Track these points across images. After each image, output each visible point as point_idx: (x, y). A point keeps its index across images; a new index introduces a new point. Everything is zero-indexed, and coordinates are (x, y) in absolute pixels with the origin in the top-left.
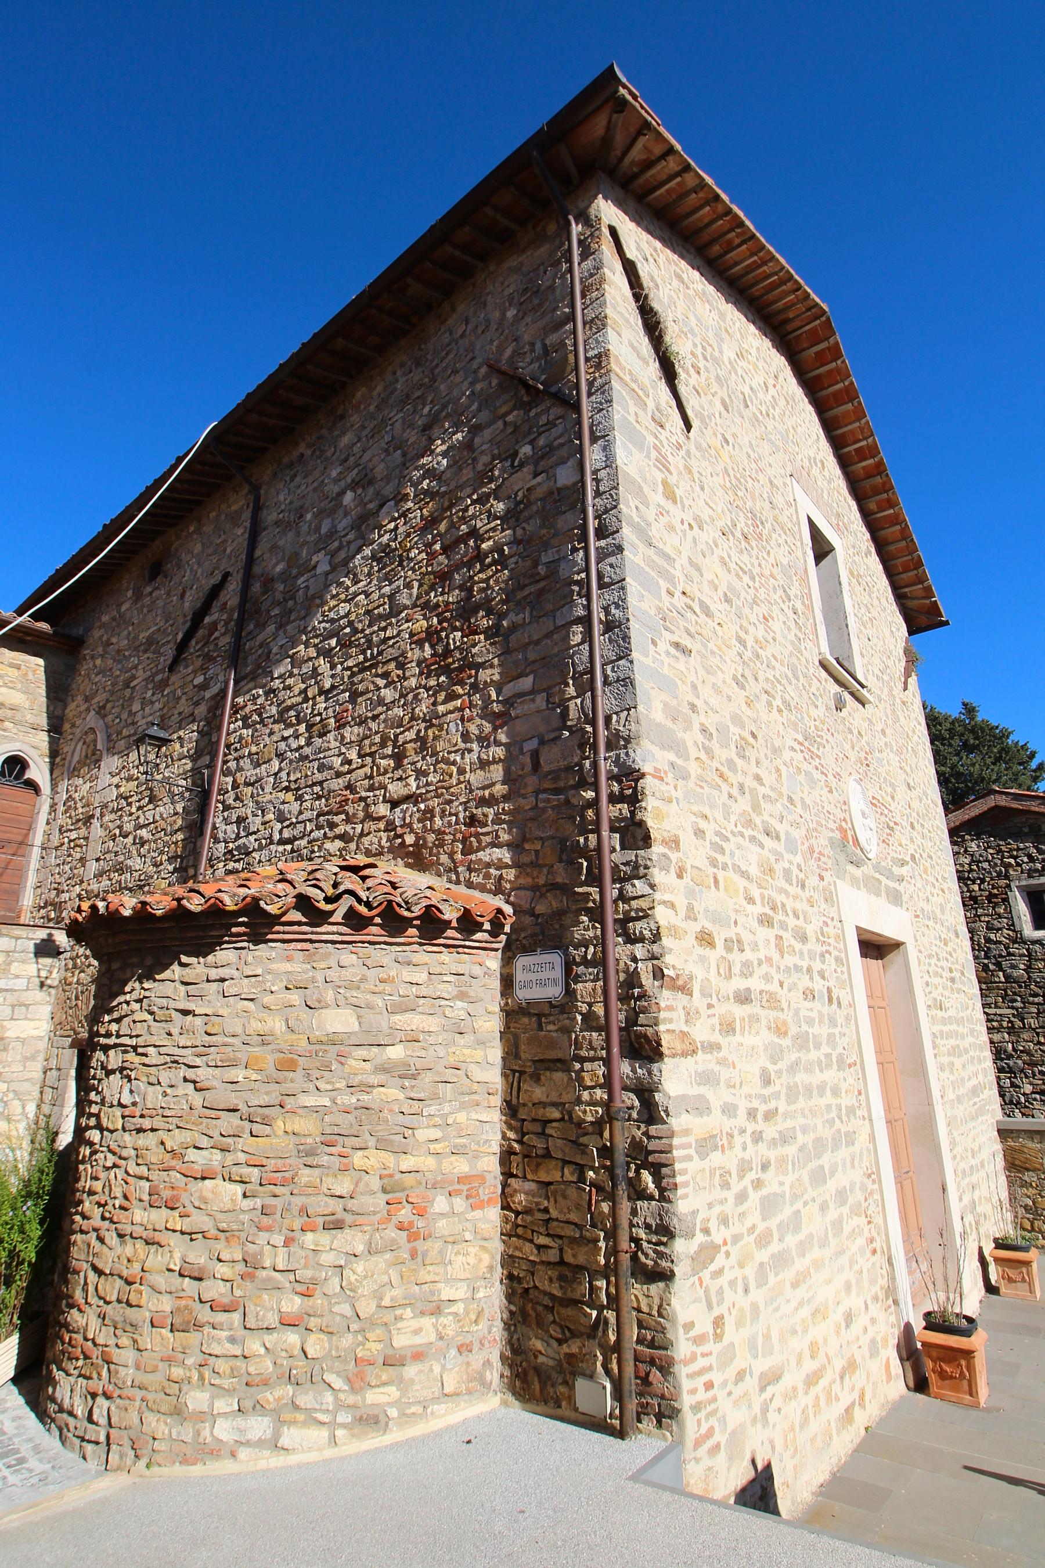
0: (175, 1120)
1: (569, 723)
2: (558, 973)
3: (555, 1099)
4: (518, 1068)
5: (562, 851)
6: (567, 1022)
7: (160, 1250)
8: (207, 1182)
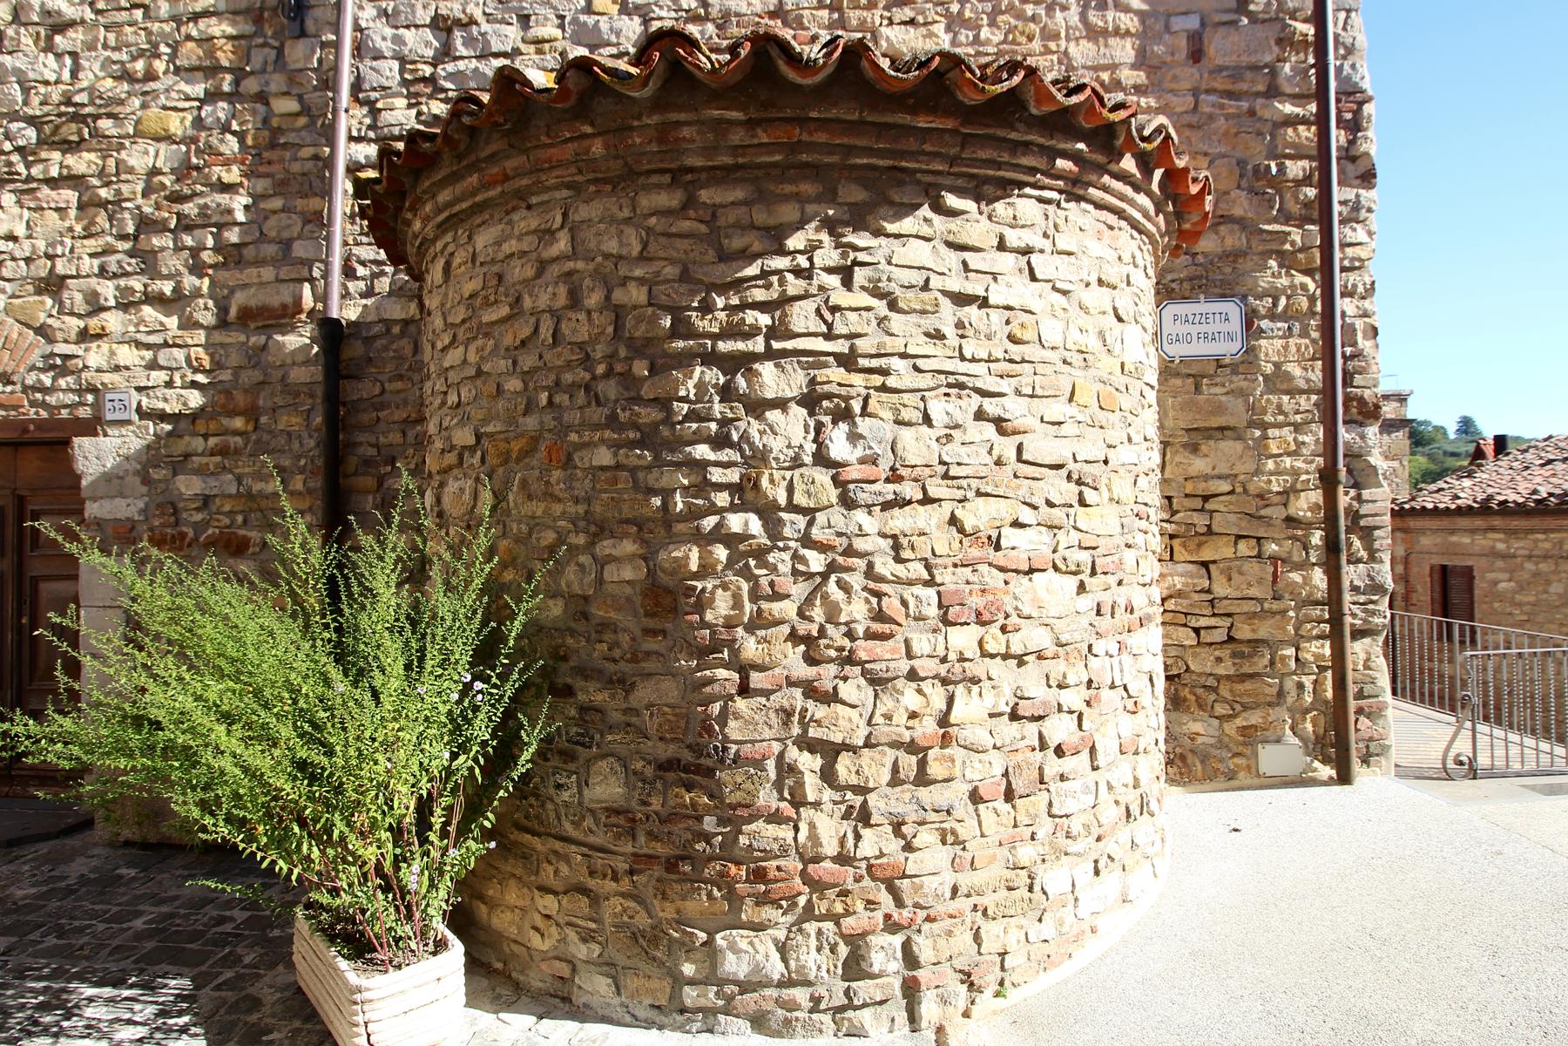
0: (975, 483)
1: (1252, 7)
2: (1235, 325)
3: (1225, 471)
4: (1184, 438)
5: (1241, 176)
6: (1244, 384)
7: (975, 689)
8: (1036, 576)
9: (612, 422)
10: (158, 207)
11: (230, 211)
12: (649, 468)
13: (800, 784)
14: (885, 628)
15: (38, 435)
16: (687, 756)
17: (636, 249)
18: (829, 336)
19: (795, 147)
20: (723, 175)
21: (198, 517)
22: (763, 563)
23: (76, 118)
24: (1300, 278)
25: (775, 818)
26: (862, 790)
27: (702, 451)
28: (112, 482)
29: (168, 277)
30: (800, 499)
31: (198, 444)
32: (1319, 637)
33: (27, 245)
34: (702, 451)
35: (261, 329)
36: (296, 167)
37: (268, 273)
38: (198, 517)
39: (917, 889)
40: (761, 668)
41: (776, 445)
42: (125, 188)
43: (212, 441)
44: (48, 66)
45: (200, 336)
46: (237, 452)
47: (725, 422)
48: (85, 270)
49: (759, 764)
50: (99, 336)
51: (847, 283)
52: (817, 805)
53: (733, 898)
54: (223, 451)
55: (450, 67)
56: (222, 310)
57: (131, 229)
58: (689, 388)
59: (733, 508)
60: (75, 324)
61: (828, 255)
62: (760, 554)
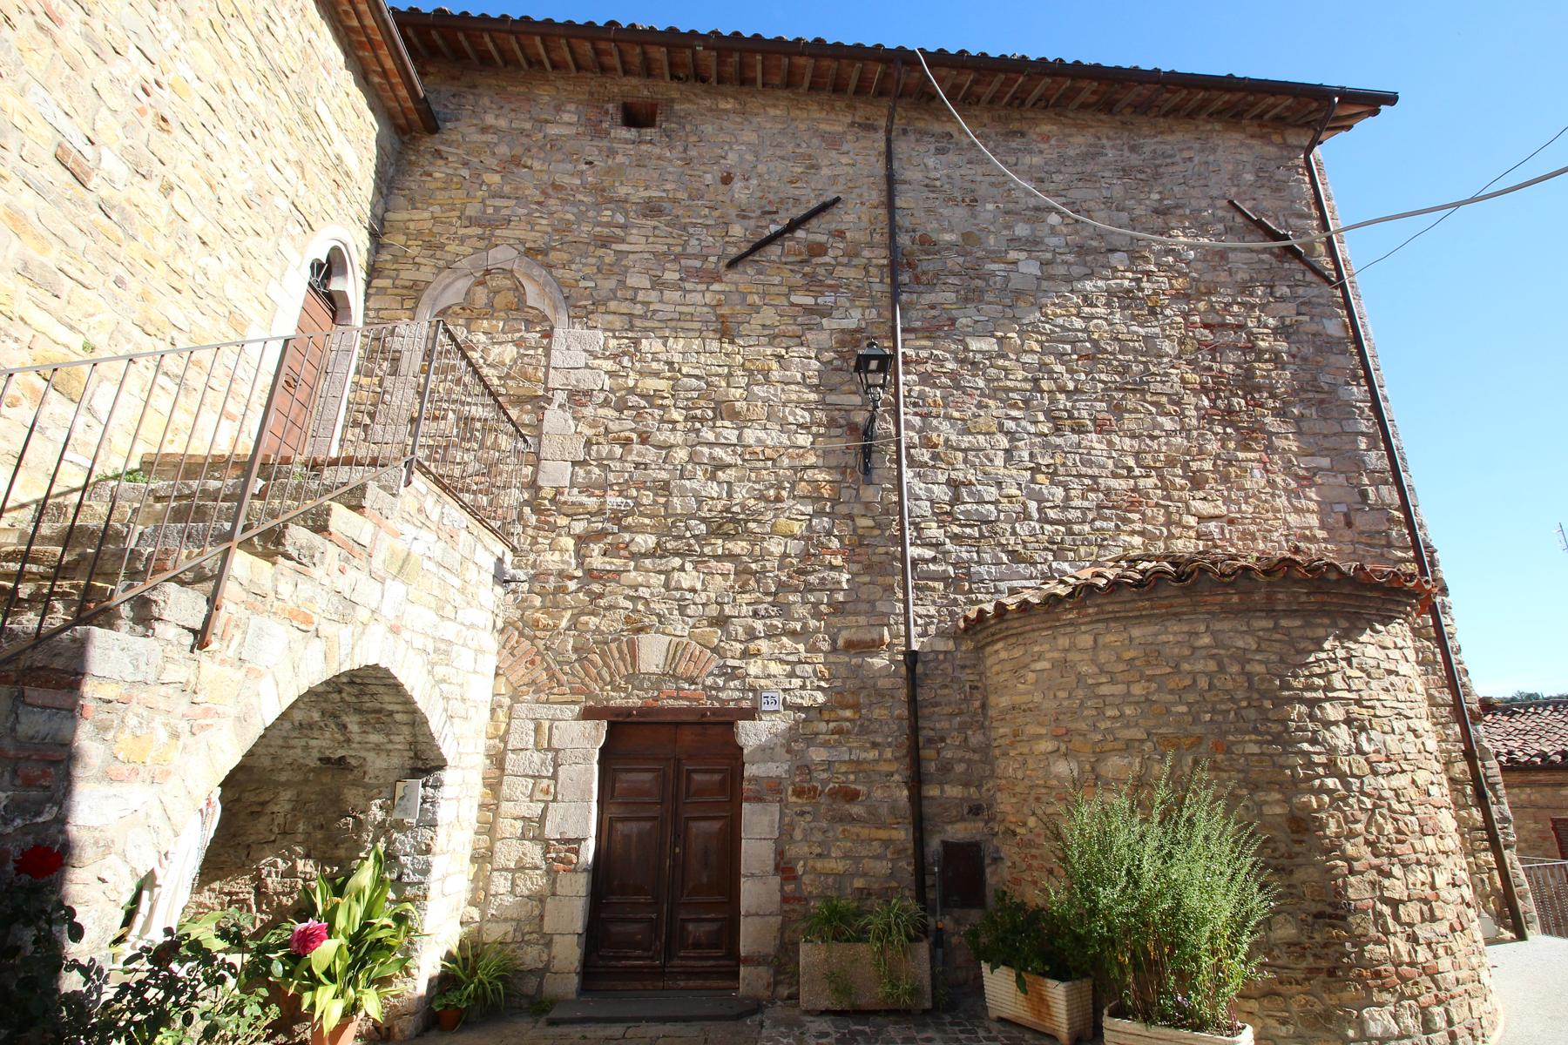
9: (1255, 731)
10: (790, 577)
11: (839, 583)
12: (1280, 755)
13: (1385, 922)
14: (1402, 837)
15: (713, 719)
16: (1329, 910)
17: (1254, 647)
18: (1350, 691)
19: (1323, 604)
20: (1289, 613)
21: (825, 776)
22: (1347, 804)
23: (732, 520)
24: (1426, 643)
25: (1378, 942)
26: (1411, 925)
27: (1306, 746)
28: (766, 751)
29: (798, 620)
30: (1355, 771)
31: (823, 727)
32: (1485, 850)
33: (703, 595)
34: (1306, 746)
35: (858, 654)
36: (875, 559)
37: (862, 620)
38: (825, 776)
39: (1444, 979)
40: (1357, 860)
41: (1340, 743)
42: (768, 564)
43: (832, 725)
44: (713, 489)
45: (821, 658)
46: (849, 732)
47: (1314, 732)
48: (744, 612)
49: (1365, 912)
50: (755, 655)
51: (1350, 665)
52: (1395, 934)
53: (1368, 988)
54: (839, 731)
55: (962, 507)
56: (834, 642)
57: (773, 589)
58: (1294, 716)
59: (1327, 776)
60: (738, 646)
61: (1341, 653)
62: (1344, 799)
